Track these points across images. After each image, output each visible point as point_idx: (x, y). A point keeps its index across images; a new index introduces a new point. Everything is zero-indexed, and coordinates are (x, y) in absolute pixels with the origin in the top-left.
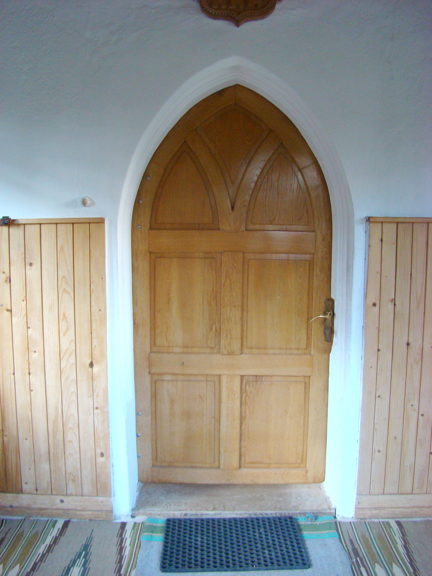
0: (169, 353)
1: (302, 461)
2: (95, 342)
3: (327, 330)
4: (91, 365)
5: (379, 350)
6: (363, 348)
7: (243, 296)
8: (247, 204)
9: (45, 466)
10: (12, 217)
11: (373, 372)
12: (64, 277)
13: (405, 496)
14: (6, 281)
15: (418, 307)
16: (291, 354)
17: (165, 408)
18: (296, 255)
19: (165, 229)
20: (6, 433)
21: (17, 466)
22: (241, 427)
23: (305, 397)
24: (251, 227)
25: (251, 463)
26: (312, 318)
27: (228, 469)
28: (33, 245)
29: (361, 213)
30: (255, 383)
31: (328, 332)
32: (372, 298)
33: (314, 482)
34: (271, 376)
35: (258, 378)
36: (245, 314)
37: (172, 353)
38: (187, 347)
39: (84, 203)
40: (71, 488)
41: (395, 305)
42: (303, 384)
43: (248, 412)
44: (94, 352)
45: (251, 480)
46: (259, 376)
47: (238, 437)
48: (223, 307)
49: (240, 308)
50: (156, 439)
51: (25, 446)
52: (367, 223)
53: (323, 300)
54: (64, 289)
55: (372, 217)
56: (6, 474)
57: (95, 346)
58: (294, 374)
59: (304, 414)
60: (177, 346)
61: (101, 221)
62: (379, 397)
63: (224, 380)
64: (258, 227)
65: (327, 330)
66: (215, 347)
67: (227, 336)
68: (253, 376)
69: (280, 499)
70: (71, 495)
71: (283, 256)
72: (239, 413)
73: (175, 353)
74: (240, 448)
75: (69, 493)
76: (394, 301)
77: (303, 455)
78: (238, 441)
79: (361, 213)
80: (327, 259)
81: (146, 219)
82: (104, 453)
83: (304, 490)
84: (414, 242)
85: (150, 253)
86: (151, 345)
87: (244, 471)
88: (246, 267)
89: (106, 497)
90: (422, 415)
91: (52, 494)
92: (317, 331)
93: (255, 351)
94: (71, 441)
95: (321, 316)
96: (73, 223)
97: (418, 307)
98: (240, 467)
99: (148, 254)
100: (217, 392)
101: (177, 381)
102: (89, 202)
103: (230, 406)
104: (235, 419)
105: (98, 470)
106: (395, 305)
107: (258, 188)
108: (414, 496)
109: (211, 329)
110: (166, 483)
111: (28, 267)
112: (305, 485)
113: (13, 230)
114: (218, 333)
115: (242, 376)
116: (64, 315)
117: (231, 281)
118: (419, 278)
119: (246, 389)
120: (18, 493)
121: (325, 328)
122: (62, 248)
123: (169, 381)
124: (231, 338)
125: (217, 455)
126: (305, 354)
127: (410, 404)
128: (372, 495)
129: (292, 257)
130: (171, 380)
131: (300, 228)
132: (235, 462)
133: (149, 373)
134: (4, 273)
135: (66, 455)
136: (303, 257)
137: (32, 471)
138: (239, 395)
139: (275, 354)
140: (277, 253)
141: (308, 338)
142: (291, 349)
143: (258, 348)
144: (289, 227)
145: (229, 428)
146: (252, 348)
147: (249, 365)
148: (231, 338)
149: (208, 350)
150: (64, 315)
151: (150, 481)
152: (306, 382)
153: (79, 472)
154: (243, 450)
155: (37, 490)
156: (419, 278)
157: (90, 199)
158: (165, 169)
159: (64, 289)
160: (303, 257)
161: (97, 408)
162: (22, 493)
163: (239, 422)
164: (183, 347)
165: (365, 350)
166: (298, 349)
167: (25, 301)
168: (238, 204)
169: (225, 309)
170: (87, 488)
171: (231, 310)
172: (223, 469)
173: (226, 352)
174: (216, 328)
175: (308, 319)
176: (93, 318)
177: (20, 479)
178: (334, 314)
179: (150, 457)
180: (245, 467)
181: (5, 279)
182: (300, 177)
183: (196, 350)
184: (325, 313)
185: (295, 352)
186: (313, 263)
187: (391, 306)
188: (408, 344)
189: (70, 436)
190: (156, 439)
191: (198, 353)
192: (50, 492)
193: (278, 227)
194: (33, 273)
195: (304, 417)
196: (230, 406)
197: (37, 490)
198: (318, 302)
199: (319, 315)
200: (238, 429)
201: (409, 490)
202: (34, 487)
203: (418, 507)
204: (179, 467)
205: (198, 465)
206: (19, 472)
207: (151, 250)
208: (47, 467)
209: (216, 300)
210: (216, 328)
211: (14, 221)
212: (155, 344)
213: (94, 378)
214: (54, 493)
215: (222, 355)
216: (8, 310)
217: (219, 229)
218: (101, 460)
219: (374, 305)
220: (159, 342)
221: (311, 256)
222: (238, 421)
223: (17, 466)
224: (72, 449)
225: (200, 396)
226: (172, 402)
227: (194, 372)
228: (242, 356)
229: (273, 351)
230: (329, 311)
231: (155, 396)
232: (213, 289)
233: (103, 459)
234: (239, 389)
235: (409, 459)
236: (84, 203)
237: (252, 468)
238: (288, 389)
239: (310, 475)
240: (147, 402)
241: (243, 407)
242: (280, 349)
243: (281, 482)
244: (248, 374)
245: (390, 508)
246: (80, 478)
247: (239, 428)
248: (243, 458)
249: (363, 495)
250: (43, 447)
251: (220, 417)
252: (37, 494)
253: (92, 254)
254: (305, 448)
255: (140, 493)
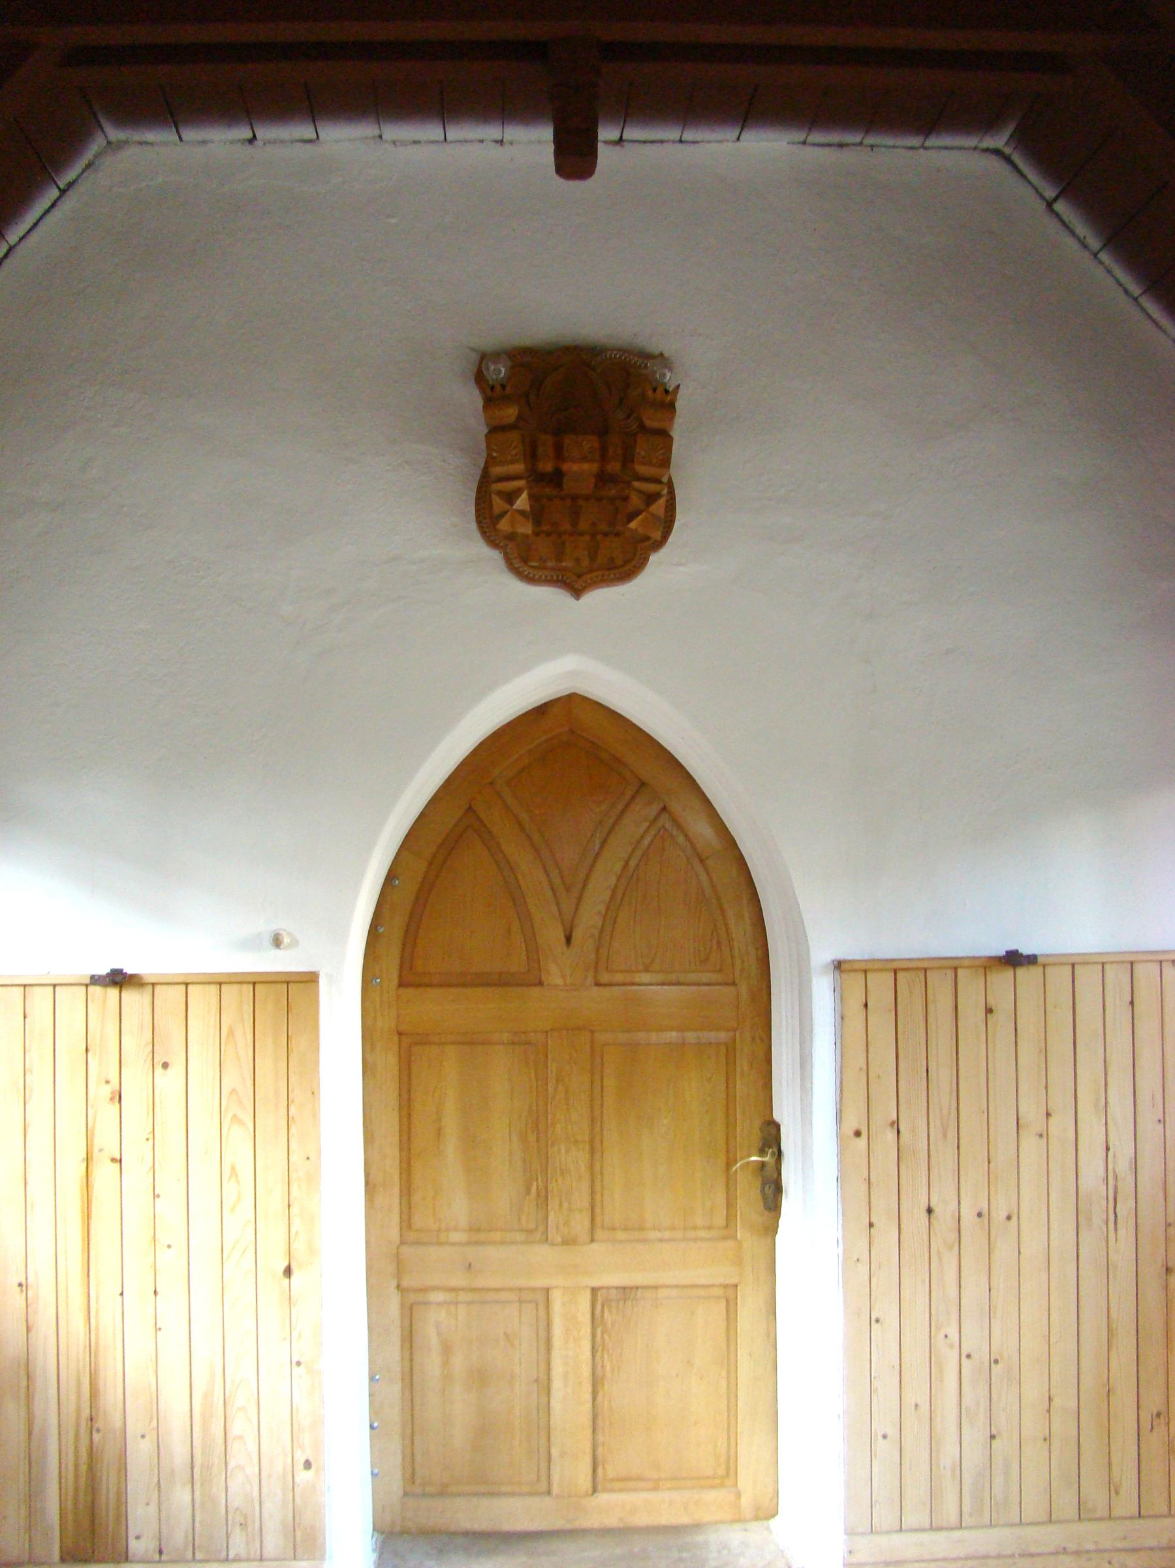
0: (439, 1244)
1: (726, 1473)
2: (297, 1224)
3: (767, 1187)
4: (288, 1272)
5: (871, 1225)
6: (841, 1222)
7: (592, 1120)
8: (596, 932)
9: (181, 1496)
10: (129, 970)
11: (863, 1269)
12: (234, 1090)
13: (944, 1534)
14: (112, 1099)
15: (945, 1135)
16: (695, 1240)
17: (431, 1364)
18: (700, 1033)
19: (430, 985)
20: (99, 1424)
21: (118, 1500)
22: (594, 1399)
23: (728, 1330)
24: (605, 978)
25: (618, 1480)
26: (736, 1162)
27: (570, 1496)
28: (171, 1025)
29: (822, 953)
30: (621, 1303)
31: (769, 1191)
32: (851, 1124)
33: (757, 1518)
34: (656, 1287)
35: (627, 1292)
36: (597, 1156)
37: (447, 1243)
38: (478, 1230)
39: (277, 942)
40: (238, 1543)
41: (898, 1132)
42: (723, 1303)
43: (608, 1367)
44: (294, 1246)
45: (621, 1519)
46: (631, 1288)
47: (586, 1420)
48: (553, 1145)
49: (587, 1146)
50: (413, 1435)
51: (140, 1452)
52: (837, 973)
53: (757, 1124)
54: (235, 1116)
55: (845, 961)
56: (93, 1522)
57: (297, 1233)
58: (703, 1281)
59: (728, 1365)
60: (456, 1229)
61: (310, 979)
62: (877, 1321)
63: (557, 1297)
64: (619, 977)
65: (767, 1187)
66: (536, 1229)
67: (561, 1205)
68: (617, 1288)
69: (684, 1555)
70: (237, 1559)
71: (673, 1035)
72: (590, 1367)
73: (453, 1244)
74: (594, 1449)
75: (232, 1555)
76: (896, 1125)
77: (729, 1457)
78: (590, 1431)
79: (822, 953)
80: (762, 1040)
81: (390, 965)
82: (311, 1460)
83: (734, 1536)
84: (931, 1007)
85: (400, 1034)
86: (401, 1229)
87: (603, 1498)
88: (598, 1060)
89: (314, 1559)
90: (968, 1356)
91: (194, 1559)
92: (748, 1191)
93: (621, 1235)
94: (240, 1437)
95: (753, 1158)
96: (255, 981)
97: (945, 1135)
98: (595, 1490)
99: (396, 1038)
100: (542, 1325)
101: (457, 1303)
102: (286, 940)
103: (571, 1354)
104: (580, 1383)
105: (298, 1501)
106: (898, 1132)
107: (619, 897)
108: (965, 1533)
109: (528, 1192)
110: (433, 1532)
111: (159, 1070)
112: (737, 1526)
113: (131, 997)
114: (543, 1199)
115: (594, 1291)
116: (233, 1169)
117: (567, 1091)
118: (943, 1075)
119: (602, 1317)
120: (119, 1562)
121: (764, 1184)
122: (231, 1032)
123: (439, 1304)
124: (570, 1210)
125: (543, 1465)
126: (724, 1238)
127: (941, 1335)
128: (877, 1533)
129: (691, 1036)
130: (445, 1303)
131: (705, 977)
132: (583, 1479)
133: (398, 1287)
134: (107, 1082)
135: (230, 1468)
136: (712, 1036)
137: (153, 1508)
138: (589, 1330)
139: (661, 1240)
140: (662, 1029)
141: (730, 1204)
142: (695, 1228)
143: (626, 1229)
144: (682, 978)
145: (569, 1403)
146: (614, 1229)
147: (609, 1266)
148: (570, 1210)
149: (520, 1237)
150: (233, 1169)
151: (398, 1528)
152: (729, 1296)
153: (257, 1508)
154: (600, 1450)
155: (161, 1552)
156: (943, 1075)
157: (289, 934)
158: (430, 864)
159: (235, 1116)
160: (712, 1036)
161: (299, 1363)
162: (127, 1560)
163: (590, 1389)
164: (470, 1230)
165: (843, 1226)
166: (710, 1228)
167: (151, 1141)
168: (578, 935)
169: (556, 1148)
170: (273, 1542)
171: (567, 1151)
172: (557, 1496)
173: (559, 1239)
174: (539, 1187)
175: (729, 1164)
176: (293, 1175)
177: (124, 1527)
178: (780, 1152)
179: (398, 1474)
180: (605, 1490)
181: (109, 1096)
182: (703, 877)
183: (497, 1236)
184: (762, 1152)
185: (703, 1234)
186: (734, 1048)
187: (891, 1135)
188: (930, 1211)
189: (239, 1426)
190: (413, 1435)
191: (503, 1243)
192: (189, 1555)
193: (660, 977)
194: (169, 1082)
195: (728, 1372)
196: (571, 1354)
197: (161, 1552)
198: (748, 1129)
199: (750, 1156)
200: (588, 1407)
201: (953, 1519)
202: (153, 1545)
203: (977, 1558)
204: (460, 1495)
205: (504, 1489)
206: (121, 1515)
207: (402, 1028)
208: (187, 1497)
209: (537, 1131)
210: (539, 1187)
211: (132, 976)
212: (410, 1227)
213: (294, 1299)
214: (199, 1555)
215: (553, 1244)
216: (113, 1160)
217: (541, 984)
218: (303, 1476)
219: (858, 1134)
220: (418, 1220)
221: (731, 1034)
222: (587, 1388)
223: (118, 1500)
224: (242, 1455)
225: (505, 1334)
226: (447, 1349)
227: (492, 1283)
228: (595, 1246)
229: (658, 1234)
230: (770, 1147)
231: (409, 1339)
232: (530, 1107)
233: (310, 1474)
234: (589, 1316)
235: (949, 1451)
236: (277, 942)
237: (621, 1490)
238: (692, 1313)
239: (745, 1501)
240: (393, 1353)
241: (599, 1354)
242: (673, 1228)
243: (685, 1520)
244: (606, 1285)
245: (917, 1561)
246: (257, 1520)
247: (590, 1400)
248: (600, 1471)
249: (858, 1534)
250: (178, 1451)
251: (549, 1379)
252: (160, 1561)
253: (293, 1043)
254: (733, 1441)
255: (380, 1556)
